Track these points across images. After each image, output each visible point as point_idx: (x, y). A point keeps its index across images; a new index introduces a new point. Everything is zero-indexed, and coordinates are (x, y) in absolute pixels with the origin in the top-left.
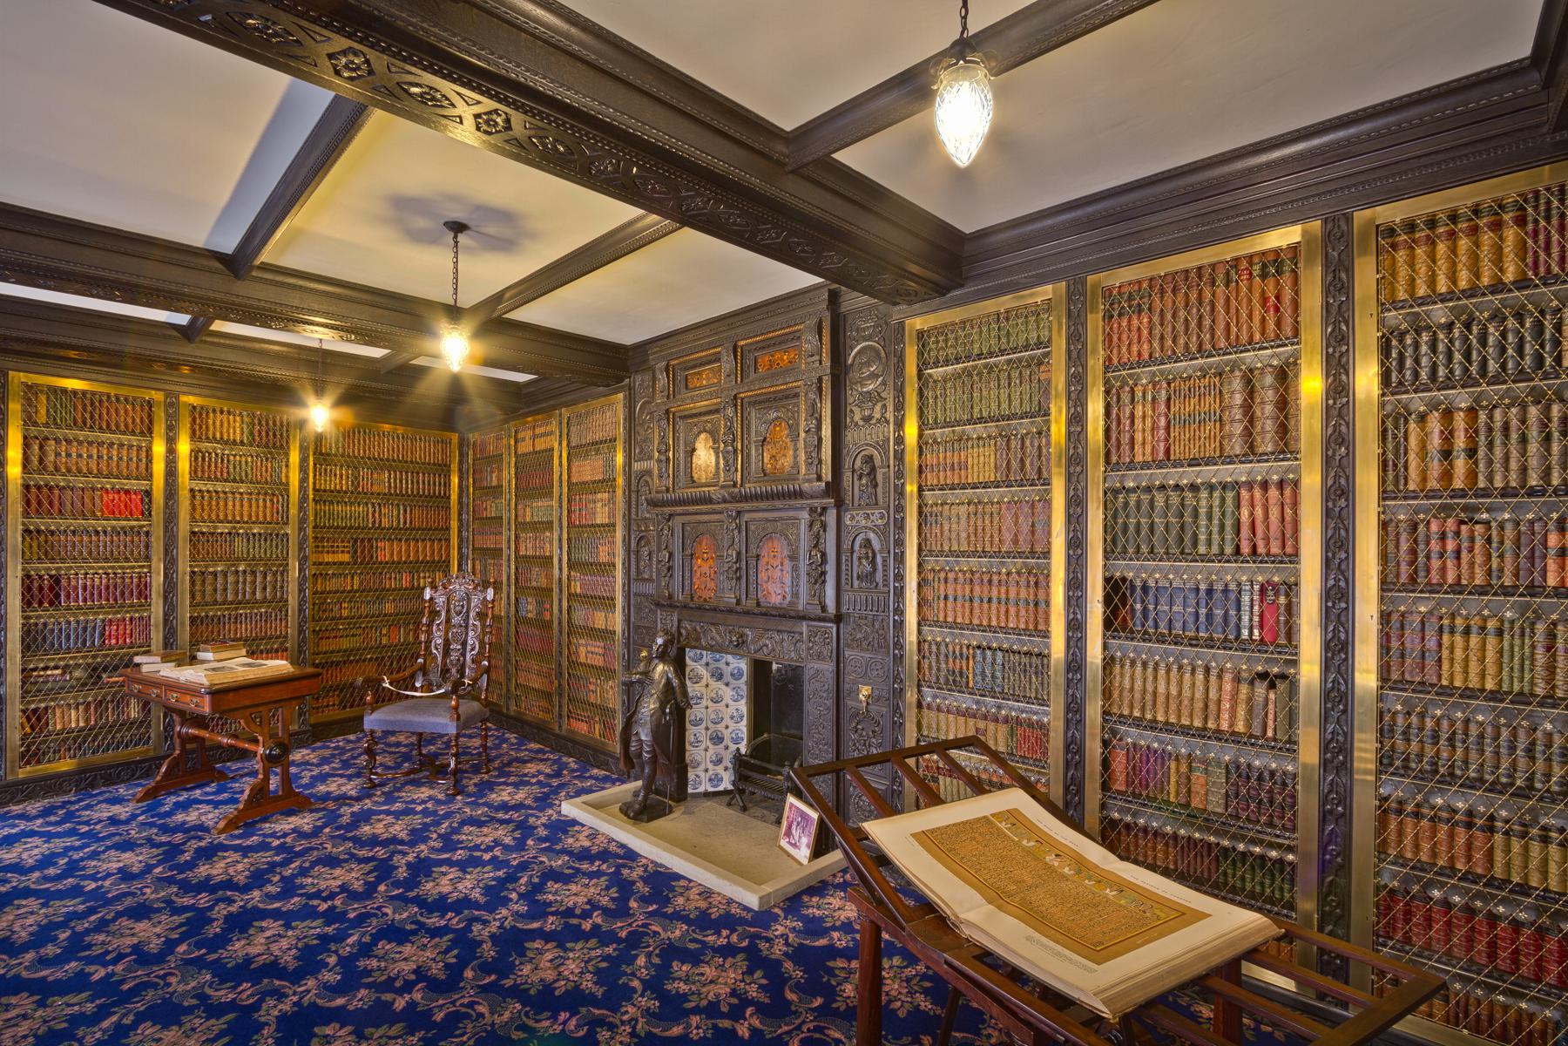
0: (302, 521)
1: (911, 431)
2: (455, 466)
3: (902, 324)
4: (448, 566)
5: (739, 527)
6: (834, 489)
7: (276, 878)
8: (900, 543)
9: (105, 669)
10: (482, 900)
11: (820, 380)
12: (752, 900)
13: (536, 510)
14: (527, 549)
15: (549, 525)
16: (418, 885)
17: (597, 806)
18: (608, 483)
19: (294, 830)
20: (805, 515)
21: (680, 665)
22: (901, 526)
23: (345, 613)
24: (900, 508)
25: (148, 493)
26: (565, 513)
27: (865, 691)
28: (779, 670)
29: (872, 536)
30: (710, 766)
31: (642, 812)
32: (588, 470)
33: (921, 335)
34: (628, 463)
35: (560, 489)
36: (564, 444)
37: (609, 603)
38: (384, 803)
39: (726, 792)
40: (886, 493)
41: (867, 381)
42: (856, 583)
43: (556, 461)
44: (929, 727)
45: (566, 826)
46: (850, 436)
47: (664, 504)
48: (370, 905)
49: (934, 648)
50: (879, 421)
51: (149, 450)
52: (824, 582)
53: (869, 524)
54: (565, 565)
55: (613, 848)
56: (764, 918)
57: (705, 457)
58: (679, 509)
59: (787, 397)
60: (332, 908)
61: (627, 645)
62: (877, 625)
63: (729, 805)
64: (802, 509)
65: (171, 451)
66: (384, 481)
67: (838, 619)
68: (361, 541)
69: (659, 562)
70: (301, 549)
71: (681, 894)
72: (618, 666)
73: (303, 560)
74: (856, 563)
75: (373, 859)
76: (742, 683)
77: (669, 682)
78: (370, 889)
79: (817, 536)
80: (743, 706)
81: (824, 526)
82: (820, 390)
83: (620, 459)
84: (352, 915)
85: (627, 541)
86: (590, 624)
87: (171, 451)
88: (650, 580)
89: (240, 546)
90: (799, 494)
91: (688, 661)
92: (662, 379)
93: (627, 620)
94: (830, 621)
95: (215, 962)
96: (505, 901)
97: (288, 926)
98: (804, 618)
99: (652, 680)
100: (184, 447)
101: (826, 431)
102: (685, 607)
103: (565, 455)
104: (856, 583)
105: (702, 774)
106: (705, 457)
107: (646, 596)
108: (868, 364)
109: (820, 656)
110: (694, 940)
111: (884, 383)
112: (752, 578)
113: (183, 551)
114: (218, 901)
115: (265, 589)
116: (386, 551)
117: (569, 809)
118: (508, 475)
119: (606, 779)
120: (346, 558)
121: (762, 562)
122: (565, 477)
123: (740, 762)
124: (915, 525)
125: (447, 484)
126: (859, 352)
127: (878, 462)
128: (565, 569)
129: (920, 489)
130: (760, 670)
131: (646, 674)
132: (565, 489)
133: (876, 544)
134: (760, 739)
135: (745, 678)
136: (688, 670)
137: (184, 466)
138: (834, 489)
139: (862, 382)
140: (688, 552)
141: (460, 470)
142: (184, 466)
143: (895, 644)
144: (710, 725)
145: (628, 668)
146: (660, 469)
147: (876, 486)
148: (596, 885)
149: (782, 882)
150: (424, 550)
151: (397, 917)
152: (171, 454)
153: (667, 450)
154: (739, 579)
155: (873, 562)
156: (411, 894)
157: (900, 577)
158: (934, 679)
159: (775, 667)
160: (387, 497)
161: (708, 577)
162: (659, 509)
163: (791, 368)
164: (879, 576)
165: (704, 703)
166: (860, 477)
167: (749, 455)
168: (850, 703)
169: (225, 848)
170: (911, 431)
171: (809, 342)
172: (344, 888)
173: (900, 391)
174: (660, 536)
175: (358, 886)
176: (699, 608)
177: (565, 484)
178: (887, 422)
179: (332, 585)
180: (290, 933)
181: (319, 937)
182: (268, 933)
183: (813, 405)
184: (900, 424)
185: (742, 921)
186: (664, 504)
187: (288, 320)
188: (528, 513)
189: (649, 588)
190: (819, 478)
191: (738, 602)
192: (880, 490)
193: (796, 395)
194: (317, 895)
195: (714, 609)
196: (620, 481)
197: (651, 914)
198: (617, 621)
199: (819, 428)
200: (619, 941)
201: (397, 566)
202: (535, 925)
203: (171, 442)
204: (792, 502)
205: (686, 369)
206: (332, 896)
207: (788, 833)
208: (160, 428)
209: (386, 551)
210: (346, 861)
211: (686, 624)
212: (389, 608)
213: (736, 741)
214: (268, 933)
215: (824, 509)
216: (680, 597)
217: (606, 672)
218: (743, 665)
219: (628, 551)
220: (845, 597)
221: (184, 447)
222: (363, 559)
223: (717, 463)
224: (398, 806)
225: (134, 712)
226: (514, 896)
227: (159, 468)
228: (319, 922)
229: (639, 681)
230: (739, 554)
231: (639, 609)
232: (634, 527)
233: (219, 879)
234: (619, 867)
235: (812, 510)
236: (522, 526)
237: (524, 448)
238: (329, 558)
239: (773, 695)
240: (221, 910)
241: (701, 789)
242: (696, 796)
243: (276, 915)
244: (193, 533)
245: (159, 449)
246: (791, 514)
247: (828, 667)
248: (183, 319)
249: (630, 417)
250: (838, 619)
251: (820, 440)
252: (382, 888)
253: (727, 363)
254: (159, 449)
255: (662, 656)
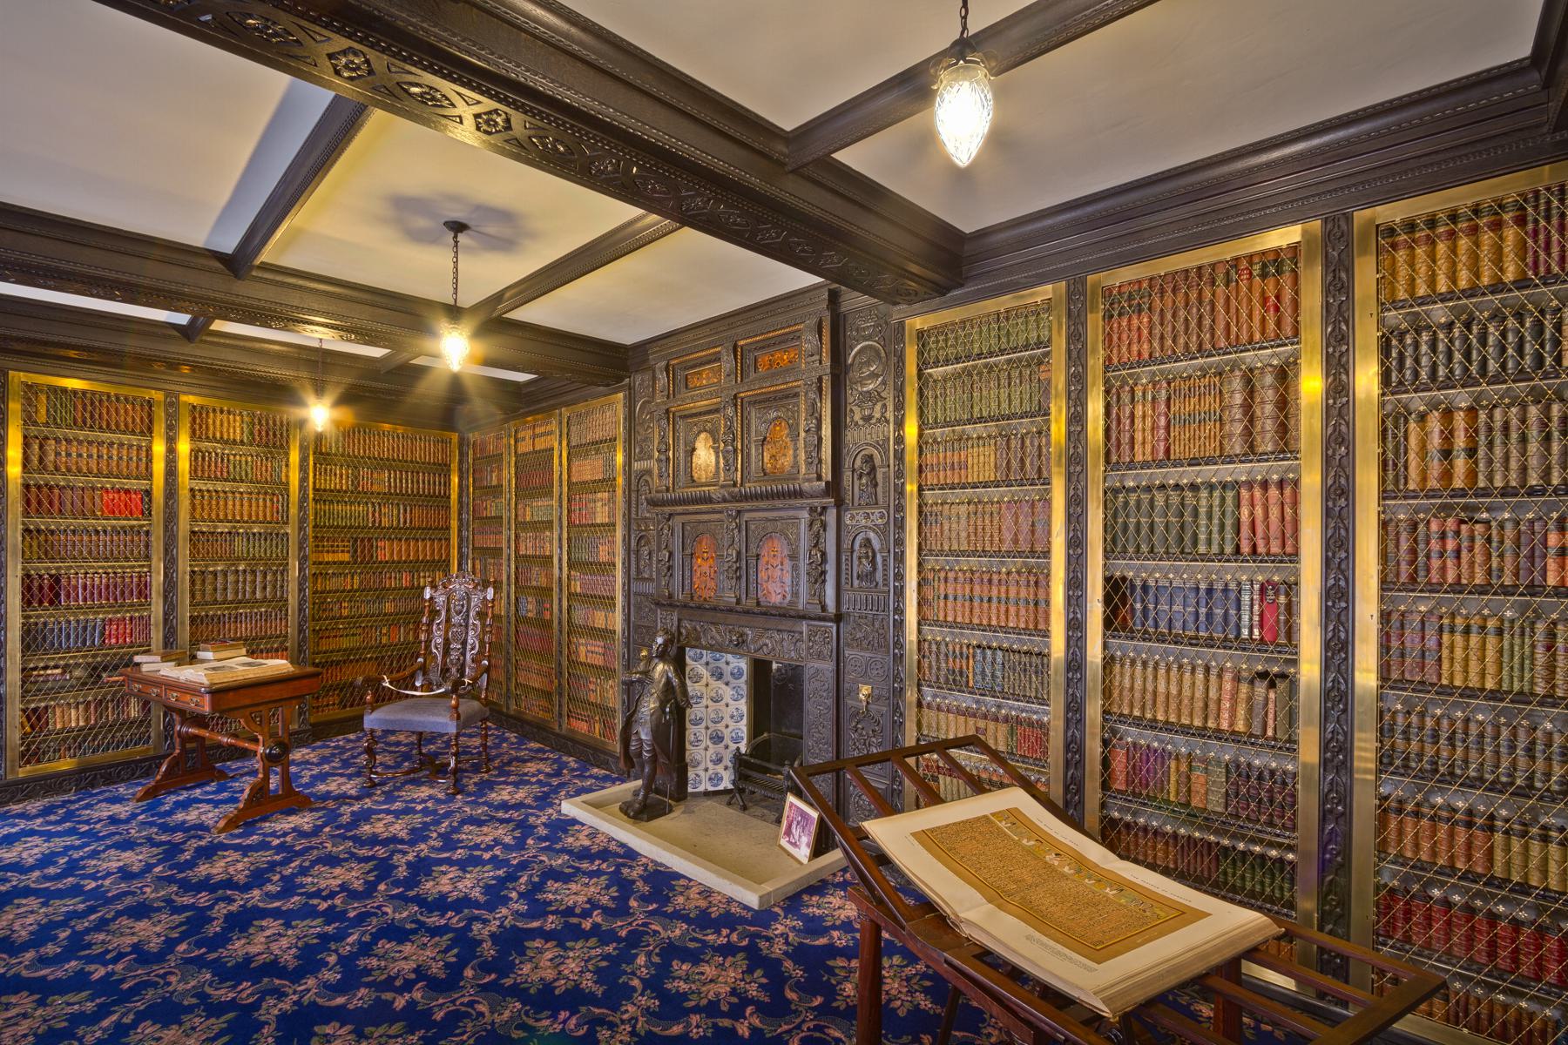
0: (302, 521)
1: (911, 430)
2: (455, 466)
3: (902, 324)
4: (448, 565)
5: (739, 527)
6: (834, 488)
7: (276, 877)
8: (900, 542)
9: (105, 669)
10: (482, 899)
11: (820, 379)
12: (752, 899)
13: (536, 509)
14: (527, 548)
15: (549, 525)
16: (418, 884)
17: (597, 805)
18: (608, 483)
19: (294, 830)
20: (805, 515)
21: (680, 664)
22: (901, 525)
23: (345, 612)
24: (900, 508)
25: (148, 493)
26: (565, 512)
27: (865, 690)
28: (779, 669)
29: (872, 535)
30: (710, 765)
31: (642, 811)
32: (588, 469)
33: (921, 334)
34: (628, 462)
35: (560, 489)
36: (564, 443)
37: (609, 602)
38: (384, 803)
39: (726, 792)
40: (886, 493)
41: (867, 381)
42: (856, 582)
43: (556, 461)
44: (929, 726)
45: (566, 825)
46: (850, 436)
47: (664, 503)
48: (370, 904)
49: (934, 647)
50: (879, 420)
51: (149, 449)
52: (824, 581)
53: (869, 524)
54: (565, 565)
55: (613, 847)
56: (764, 917)
57: (705, 456)
58: (679, 509)
59: (787, 397)
60: (332, 907)
61: (627, 644)
62: (877, 624)
63: (729, 804)
64: (802, 508)
65: (171, 451)
66: (384, 480)
67: (838, 618)
68: (361, 540)
69: (659, 561)
70: (301, 548)
71: (681, 893)
72: (618, 665)
73: (303, 560)
74: (856, 562)
75: (373, 858)
76: (742, 683)
77: (669, 682)
78: (370, 888)
79: (817, 536)
80: (743, 706)
81: (824, 526)
82: (820, 389)
83: (620, 458)
84: (352, 915)
85: (627, 540)
86: (590, 624)
87: (171, 451)
88: (650, 579)
89: (240, 546)
90: (799, 494)
91: (688, 660)
92: (662, 379)
93: (627, 620)
94: (830, 620)
95: (215, 961)
96: (505, 901)
97: (288, 925)
98: (804, 617)
99: (652, 679)
100: (184, 447)
101: (826, 431)
102: (685, 606)
103: (565, 455)
104: (856, 582)
105: (702, 773)
106: (705, 456)
107: (646, 595)
108: (868, 364)
109: (820, 656)
110: (694, 940)
111: (884, 383)
112: (752, 578)
113: (183, 551)
114: (218, 900)
115: (265, 588)
116: (386, 551)
117: (569, 808)
118: (508, 474)
119: (606, 778)
120: (346, 557)
121: (762, 561)
122: (565, 476)
123: (740, 761)
124: (915, 525)
125: (447, 484)
126: (859, 352)
127: (878, 461)
128: (565, 569)
129: (920, 489)
130: (760, 669)
131: (646, 673)
132: (565, 489)
133: (876, 544)
134: (760, 739)
135: (745, 678)
136: (688, 669)
137: (184, 465)
138: (834, 488)
139: (862, 382)
140: (688, 551)
141: (460, 470)
142: (184, 465)
143: (895, 643)
144: (710, 725)
145: (628, 667)
146: (660, 469)
147: (876, 485)
148: (596, 884)
149: (782, 881)
150: (424, 550)
151: (397, 916)
152: (171, 453)
153: (667, 450)
154: (739, 578)
155: (873, 562)
156: (411, 893)
157: (900, 577)
158: (934, 679)
159: (775, 666)
160: (387, 497)
161: (708, 576)
162: (659, 509)
163: (791, 368)
164: (879, 576)
165: (704, 702)
166: (860, 477)
167: (749, 455)
168: (850, 702)
169: (225, 847)
170: (911, 430)
171: (809, 342)
172: (344, 887)
173: (900, 391)
174: (660, 535)
175: (358, 885)
176: (699, 608)
177: (565, 483)
178: (887, 422)
179: (332, 584)
180: (290, 932)
181: (319, 936)
182: (268, 933)
183: (813, 405)
184: (900, 424)
185: (742, 921)
186: (664, 503)
187: (288, 320)
188: (528, 513)
189: (649, 588)
190: (819, 478)
191: (738, 602)
192: (880, 489)
193: (796, 395)
194: (317, 894)
195: (714, 609)
196: (620, 481)
197: (651, 913)
198: (617, 621)
199: (819, 427)
200: (619, 940)
201: (397, 565)
202: (535, 924)
203: (171, 441)
204: (792, 502)
205: (686, 369)
206: (332, 895)
207: (788, 833)
208: (160, 428)
209: (386, 551)
210: (346, 860)
211: (686, 623)
212: (389, 607)
213: (736, 740)
214: (268, 933)
215: (824, 508)
216: (680, 596)
217: (606, 671)
218: (743, 664)
219: (628, 550)
220: (845, 597)
221: (184, 447)
222: (363, 558)
223: (717, 462)
224: (398, 805)
225: (134, 711)
226: (514, 895)
227: (159, 467)
228: (319, 921)
229: (639, 681)
230: (739, 553)
231: (639, 608)
232: (634, 527)
233: (219, 878)
234: (619, 866)
235: (812, 510)
236: (522, 526)
237: (524, 447)
238: (329, 558)
239: (773, 695)
240: (221, 910)
241: (701, 789)
242: (696, 795)
243: (276, 914)
244: (193, 532)
245: (159, 448)
246: (791, 513)
247: (828, 666)
248: (183, 319)
249: (630, 417)
250: (838, 618)
251: (820, 439)
252: (382, 887)
253: (727, 362)
254: (159, 448)
255: (662, 656)
